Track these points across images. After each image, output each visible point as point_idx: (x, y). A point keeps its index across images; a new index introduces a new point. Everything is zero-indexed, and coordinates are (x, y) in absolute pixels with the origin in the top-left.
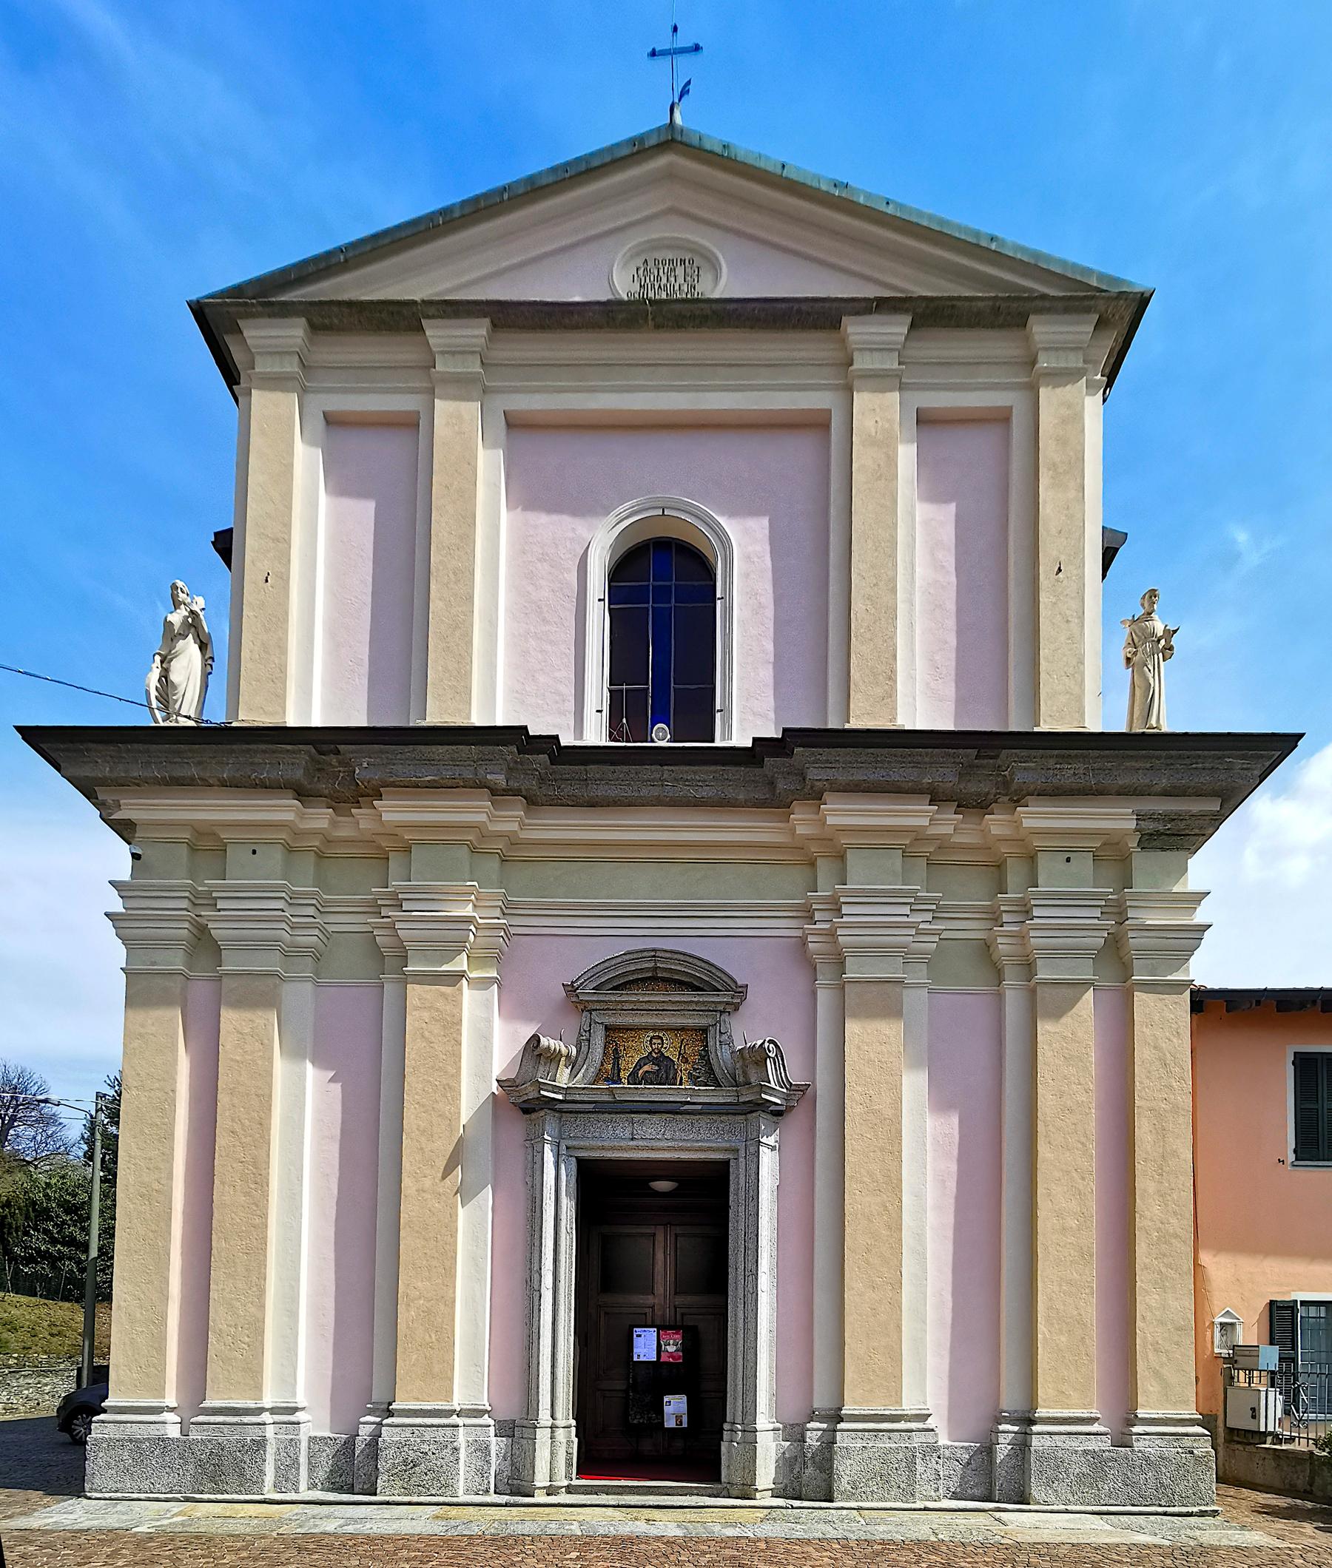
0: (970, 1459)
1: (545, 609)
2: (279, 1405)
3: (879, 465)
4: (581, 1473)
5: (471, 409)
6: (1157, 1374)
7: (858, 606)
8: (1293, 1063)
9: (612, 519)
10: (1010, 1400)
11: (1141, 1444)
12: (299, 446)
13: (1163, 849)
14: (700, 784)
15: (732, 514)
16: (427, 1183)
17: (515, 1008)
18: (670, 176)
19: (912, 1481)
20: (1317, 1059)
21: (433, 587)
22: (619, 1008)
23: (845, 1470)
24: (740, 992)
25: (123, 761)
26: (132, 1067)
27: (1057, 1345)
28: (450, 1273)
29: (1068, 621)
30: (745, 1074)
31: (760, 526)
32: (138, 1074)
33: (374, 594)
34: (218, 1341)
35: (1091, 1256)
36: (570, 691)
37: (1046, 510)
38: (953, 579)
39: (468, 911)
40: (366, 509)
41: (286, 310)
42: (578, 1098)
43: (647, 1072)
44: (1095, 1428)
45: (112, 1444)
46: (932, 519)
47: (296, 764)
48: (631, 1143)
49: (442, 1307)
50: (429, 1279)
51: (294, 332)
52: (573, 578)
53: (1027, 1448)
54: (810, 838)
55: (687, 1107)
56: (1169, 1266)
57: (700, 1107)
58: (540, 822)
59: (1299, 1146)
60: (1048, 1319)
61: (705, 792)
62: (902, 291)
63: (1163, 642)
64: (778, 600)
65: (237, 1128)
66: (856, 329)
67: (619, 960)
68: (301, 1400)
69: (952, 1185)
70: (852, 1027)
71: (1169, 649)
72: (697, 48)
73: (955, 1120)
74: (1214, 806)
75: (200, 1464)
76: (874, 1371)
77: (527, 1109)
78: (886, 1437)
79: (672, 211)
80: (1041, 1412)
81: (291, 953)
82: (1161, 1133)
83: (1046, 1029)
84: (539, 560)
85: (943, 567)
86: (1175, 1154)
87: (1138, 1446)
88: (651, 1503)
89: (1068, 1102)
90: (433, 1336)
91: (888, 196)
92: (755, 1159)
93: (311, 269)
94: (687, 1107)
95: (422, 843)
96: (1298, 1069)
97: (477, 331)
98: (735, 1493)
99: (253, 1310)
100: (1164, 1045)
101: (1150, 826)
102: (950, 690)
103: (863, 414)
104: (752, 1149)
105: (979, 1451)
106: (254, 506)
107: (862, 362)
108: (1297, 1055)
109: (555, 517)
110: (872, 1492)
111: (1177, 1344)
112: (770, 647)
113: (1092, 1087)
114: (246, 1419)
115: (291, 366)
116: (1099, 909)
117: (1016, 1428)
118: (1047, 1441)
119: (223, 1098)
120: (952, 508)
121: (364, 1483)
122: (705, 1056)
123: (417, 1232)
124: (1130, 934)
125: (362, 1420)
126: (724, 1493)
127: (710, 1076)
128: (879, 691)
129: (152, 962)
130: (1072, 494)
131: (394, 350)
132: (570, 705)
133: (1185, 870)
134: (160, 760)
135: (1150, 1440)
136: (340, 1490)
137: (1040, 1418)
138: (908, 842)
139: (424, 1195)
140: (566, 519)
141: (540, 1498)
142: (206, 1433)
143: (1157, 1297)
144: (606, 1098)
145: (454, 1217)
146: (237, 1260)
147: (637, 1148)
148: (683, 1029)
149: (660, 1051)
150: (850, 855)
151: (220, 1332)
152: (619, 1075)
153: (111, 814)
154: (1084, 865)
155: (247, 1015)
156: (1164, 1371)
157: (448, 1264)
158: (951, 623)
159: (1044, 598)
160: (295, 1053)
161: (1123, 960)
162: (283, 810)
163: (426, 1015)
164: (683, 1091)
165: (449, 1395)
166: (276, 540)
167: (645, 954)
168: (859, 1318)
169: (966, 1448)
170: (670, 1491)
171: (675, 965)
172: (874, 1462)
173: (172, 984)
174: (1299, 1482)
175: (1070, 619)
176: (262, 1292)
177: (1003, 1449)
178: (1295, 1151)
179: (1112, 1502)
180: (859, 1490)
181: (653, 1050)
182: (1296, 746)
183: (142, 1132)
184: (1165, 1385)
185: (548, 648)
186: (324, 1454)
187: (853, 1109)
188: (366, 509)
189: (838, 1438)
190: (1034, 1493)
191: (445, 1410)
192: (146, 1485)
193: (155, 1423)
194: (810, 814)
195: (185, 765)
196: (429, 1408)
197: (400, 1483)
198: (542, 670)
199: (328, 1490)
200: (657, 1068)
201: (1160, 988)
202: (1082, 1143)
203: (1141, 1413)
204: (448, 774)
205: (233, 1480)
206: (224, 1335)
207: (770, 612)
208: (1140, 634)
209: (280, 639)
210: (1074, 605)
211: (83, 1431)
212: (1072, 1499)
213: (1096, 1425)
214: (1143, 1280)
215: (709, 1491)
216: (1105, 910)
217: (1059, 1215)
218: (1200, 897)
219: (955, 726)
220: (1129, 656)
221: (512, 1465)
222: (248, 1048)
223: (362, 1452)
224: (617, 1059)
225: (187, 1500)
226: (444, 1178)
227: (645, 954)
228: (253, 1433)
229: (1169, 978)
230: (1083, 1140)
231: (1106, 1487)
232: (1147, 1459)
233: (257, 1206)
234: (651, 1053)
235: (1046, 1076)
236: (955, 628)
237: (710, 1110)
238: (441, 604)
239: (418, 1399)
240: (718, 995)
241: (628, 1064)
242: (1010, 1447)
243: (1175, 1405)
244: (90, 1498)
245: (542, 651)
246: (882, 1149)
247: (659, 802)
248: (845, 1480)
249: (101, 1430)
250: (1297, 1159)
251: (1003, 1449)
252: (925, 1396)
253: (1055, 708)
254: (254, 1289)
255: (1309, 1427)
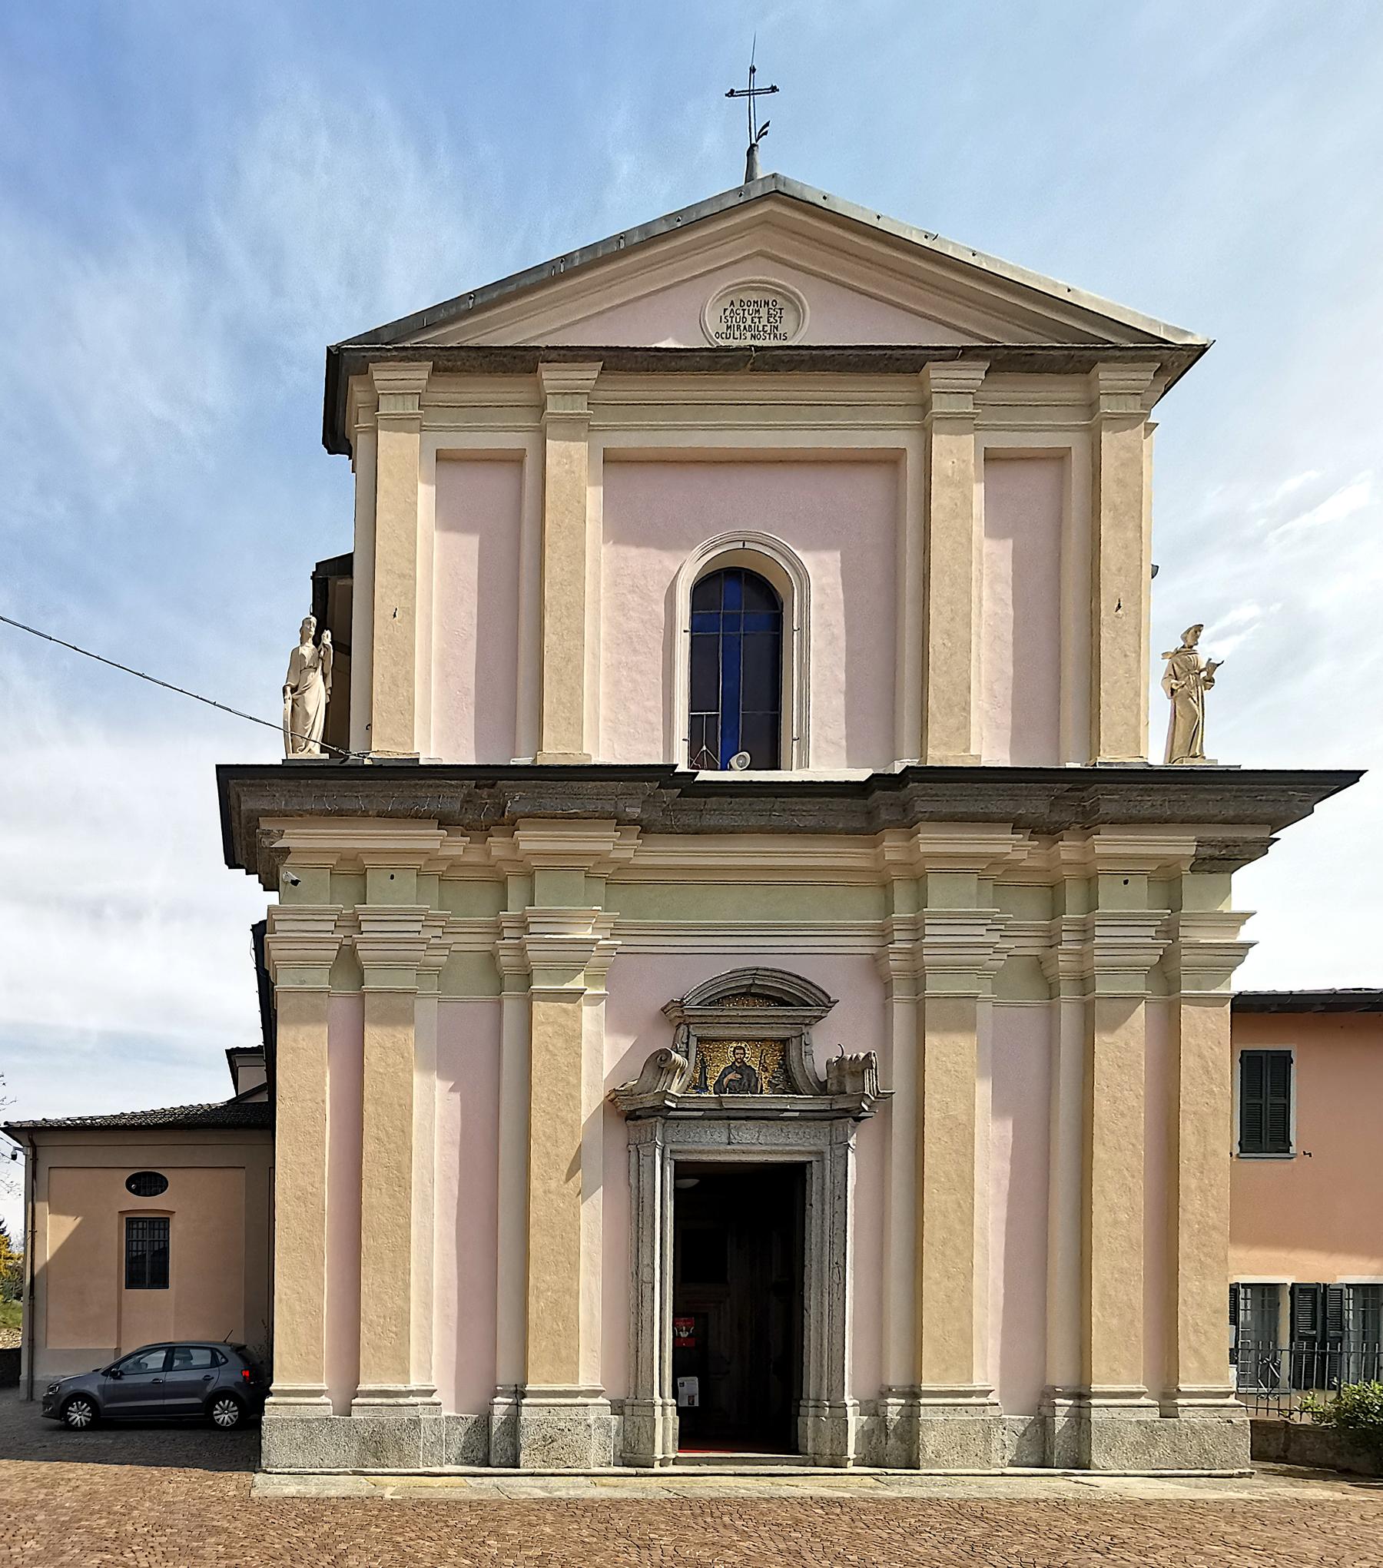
0: (1025, 1431)
1: (635, 640)
2: (419, 1388)
3: (956, 505)
4: (681, 1448)
5: (579, 449)
6: (1196, 1351)
7: (936, 640)
8: (1241, 1061)
9: (697, 551)
10: (505, 1377)
11: (1186, 1414)
12: (422, 488)
13: (1211, 872)
14: (804, 813)
15: (806, 549)
16: (553, 1184)
17: (618, 1023)
18: (765, 221)
19: (987, 1451)
20: (1261, 1057)
21: (547, 621)
22: (717, 1021)
23: (930, 1441)
24: (827, 1003)
25: (299, 794)
26: (286, 1079)
27: (1109, 1328)
28: (574, 1267)
29: (1126, 656)
30: (841, 1083)
31: (832, 560)
32: (292, 1086)
33: (480, 626)
34: (369, 1332)
35: (1140, 1247)
36: (658, 719)
37: (1107, 549)
38: (1011, 611)
39: (587, 934)
40: (470, 544)
41: (416, 354)
42: (688, 1106)
43: (731, 1080)
44: (1143, 1401)
45: (284, 1424)
46: (992, 554)
47: (451, 800)
48: (729, 1147)
49: (567, 1297)
50: (556, 1273)
51: (419, 374)
52: (661, 609)
53: (914, 1420)
54: (894, 863)
55: (786, 1114)
56: (1206, 1255)
57: (797, 1114)
58: (649, 849)
59: (1244, 1139)
60: (1102, 1305)
61: (810, 822)
62: (986, 340)
63: (1204, 674)
64: (849, 631)
65: (382, 1135)
66: (938, 374)
67: (724, 978)
68: (434, 1384)
69: (1006, 1183)
70: (932, 1040)
71: (1210, 681)
72: (774, 89)
73: (1010, 1125)
74: (1262, 833)
75: (364, 1441)
76: (948, 1352)
77: (632, 1116)
78: (964, 1411)
79: (761, 254)
80: (926, 1386)
81: (423, 971)
82: (1202, 1133)
83: (1102, 1040)
84: (630, 592)
85: (1002, 600)
86: (1215, 1153)
87: (1184, 1415)
88: (764, 1472)
89: (1120, 1107)
90: (560, 1324)
91: (927, 230)
92: (843, 1162)
93: (443, 315)
94: (786, 1114)
95: (544, 869)
96: (1245, 1067)
97: (590, 373)
98: (824, 1462)
99: (399, 1302)
100: (1206, 1053)
101: (1207, 851)
102: (1007, 719)
103: (941, 455)
104: (839, 1152)
105: (1033, 1423)
106: (381, 543)
107: (939, 406)
108: (1245, 1054)
109: (643, 550)
110: (953, 1460)
111: (1214, 1325)
112: (842, 677)
113: (1142, 1093)
114: (401, 1401)
115: (411, 407)
116: (1154, 929)
117: (1071, 1402)
118: (1105, 1414)
119: (368, 1108)
120: (1010, 543)
121: (501, 1458)
122: (785, 1067)
123: (544, 1230)
124: (1183, 952)
125: (354, 1401)
126: (811, 1462)
127: (788, 1082)
128: (953, 722)
129: (301, 981)
130: (1130, 534)
131: (510, 390)
132: (659, 734)
133: (1228, 890)
134: (332, 793)
135: (1193, 1411)
136: (472, 1463)
137: (1095, 1392)
138: (999, 873)
139: (550, 1195)
140: (654, 552)
141: (657, 1469)
142: (366, 1413)
143: (1197, 1283)
144: (713, 1106)
145: (576, 1216)
146: (384, 1257)
147: (734, 1152)
148: (763, 1040)
149: (743, 1061)
150: (932, 881)
151: (371, 1324)
152: (705, 1083)
153: (273, 843)
154: (1140, 887)
155: (389, 1030)
156: (1204, 1350)
157: (573, 1258)
158: (1009, 653)
159: (1105, 633)
160: (426, 1068)
161: (1167, 975)
162: (428, 839)
163: (550, 1030)
164: (766, 1098)
165: (575, 1378)
166: (402, 576)
167: (748, 972)
168: (936, 1304)
169: (1022, 1421)
170: (763, 1461)
171: (772, 981)
172: (955, 1434)
173: (319, 1002)
174: (1270, 1448)
175: (1128, 653)
176: (407, 1286)
177: (1060, 1421)
178: (1240, 1144)
179: (1161, 1466)
180: (942, 1458)
181: (736, 1060)
182: (1358, 781)
183: (296, 1139)
184: (1203, 1362)
185: (638, 677)
186: (457, 1432)
187: (931, 1115)
188: (470, 544)
189: (922, 1412)
190: (1094, 1459)
191: (575, 1391)
192: (316, 1460)
193: (321, 1405)
194: (902, 841)
195: (354, 799)
196: (561, 1389)
197: (540, 1457)
198: (633, 699)
199: (462, 1464)
200: (739, 1076)
201: (1205, 1001)
202: (1133, 1145)
203: (361, 1387)
204: (591, 807)
205: (392, 1455)
206: (375, 1325)
207: (842, 643)
208: (1183, 666)
209: (407, 672)
210: (1131, 640)
211: (79, 1418)
212: (1127, 1465)
213: (1143, 1398)
214: (1184, 1269)
215: (797, 1462)
216: (613, 932)
217: (1111, 1210)
218: (1244, 917)
219: (1013, 754)
220: (1174, 687)
221: (624, 1440)
222: (390, 1061)
223: (499, 1429)
224: (704, 1068)
225: (355, 1473)
226: (568, 1180)
227: (748, 972)
228: (408, 1414)
229: (1212, 992)
230: (1134, 1141)
231: (1157, 1453)
232: (1192, 1428)
233: (401, 1207)
234: (734, 1063)
235: (1102, 1083)
236: (1011, 658)
237: (806, 1117)
238: (554, 638)
239: (547, 1382)
240: (810, 1010)
241: (714, 1073)
242: (1066, 1419)
243: (1211, 1380)
244: (270, 1473)
245: (633, 681)
246: (957, 1152)
247: (761, 830)
248: (929, 1450)
249: (273, 1411)
250: (1241, 1152)
251: (1060, 1421)
252: (987, 1375)
253: (1113, 738)
254: (400, 1283)
255: (1281, 1400)
